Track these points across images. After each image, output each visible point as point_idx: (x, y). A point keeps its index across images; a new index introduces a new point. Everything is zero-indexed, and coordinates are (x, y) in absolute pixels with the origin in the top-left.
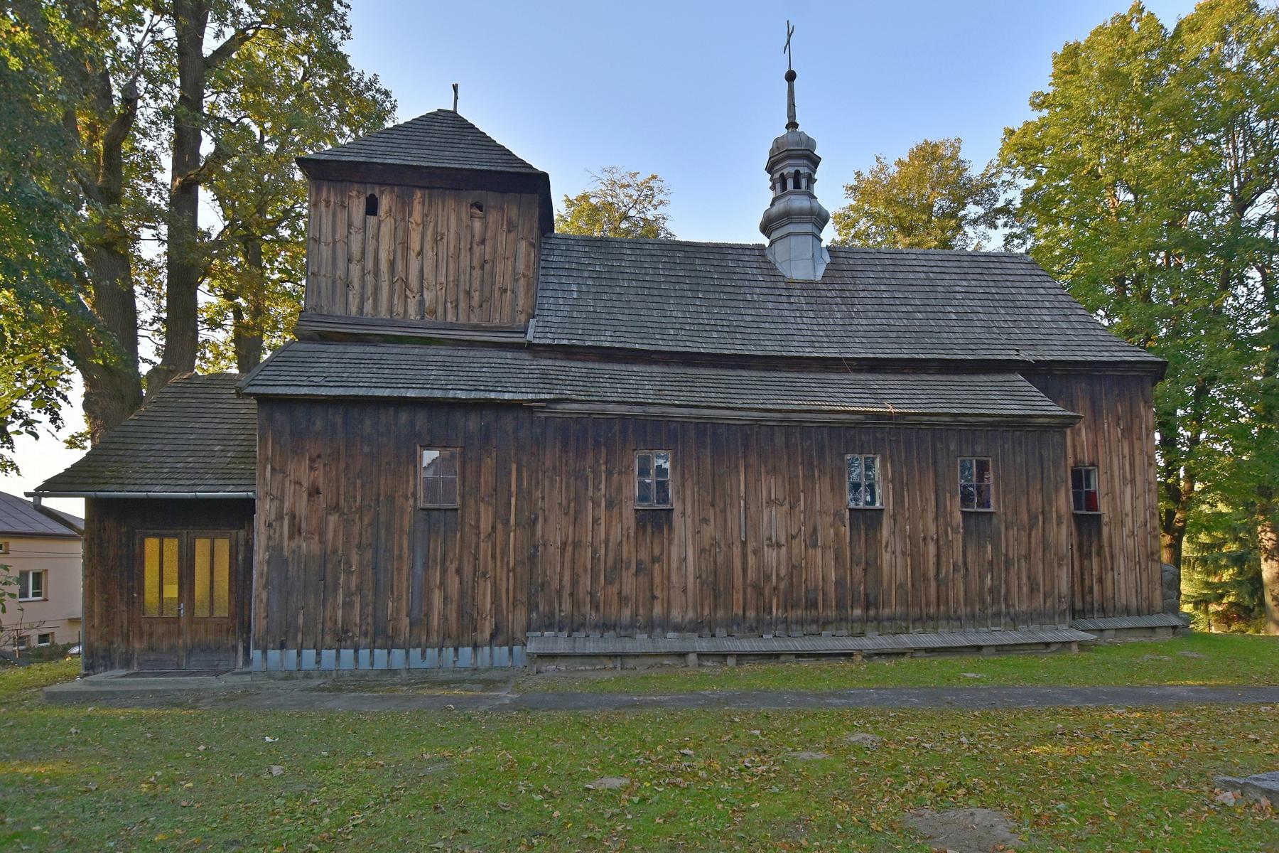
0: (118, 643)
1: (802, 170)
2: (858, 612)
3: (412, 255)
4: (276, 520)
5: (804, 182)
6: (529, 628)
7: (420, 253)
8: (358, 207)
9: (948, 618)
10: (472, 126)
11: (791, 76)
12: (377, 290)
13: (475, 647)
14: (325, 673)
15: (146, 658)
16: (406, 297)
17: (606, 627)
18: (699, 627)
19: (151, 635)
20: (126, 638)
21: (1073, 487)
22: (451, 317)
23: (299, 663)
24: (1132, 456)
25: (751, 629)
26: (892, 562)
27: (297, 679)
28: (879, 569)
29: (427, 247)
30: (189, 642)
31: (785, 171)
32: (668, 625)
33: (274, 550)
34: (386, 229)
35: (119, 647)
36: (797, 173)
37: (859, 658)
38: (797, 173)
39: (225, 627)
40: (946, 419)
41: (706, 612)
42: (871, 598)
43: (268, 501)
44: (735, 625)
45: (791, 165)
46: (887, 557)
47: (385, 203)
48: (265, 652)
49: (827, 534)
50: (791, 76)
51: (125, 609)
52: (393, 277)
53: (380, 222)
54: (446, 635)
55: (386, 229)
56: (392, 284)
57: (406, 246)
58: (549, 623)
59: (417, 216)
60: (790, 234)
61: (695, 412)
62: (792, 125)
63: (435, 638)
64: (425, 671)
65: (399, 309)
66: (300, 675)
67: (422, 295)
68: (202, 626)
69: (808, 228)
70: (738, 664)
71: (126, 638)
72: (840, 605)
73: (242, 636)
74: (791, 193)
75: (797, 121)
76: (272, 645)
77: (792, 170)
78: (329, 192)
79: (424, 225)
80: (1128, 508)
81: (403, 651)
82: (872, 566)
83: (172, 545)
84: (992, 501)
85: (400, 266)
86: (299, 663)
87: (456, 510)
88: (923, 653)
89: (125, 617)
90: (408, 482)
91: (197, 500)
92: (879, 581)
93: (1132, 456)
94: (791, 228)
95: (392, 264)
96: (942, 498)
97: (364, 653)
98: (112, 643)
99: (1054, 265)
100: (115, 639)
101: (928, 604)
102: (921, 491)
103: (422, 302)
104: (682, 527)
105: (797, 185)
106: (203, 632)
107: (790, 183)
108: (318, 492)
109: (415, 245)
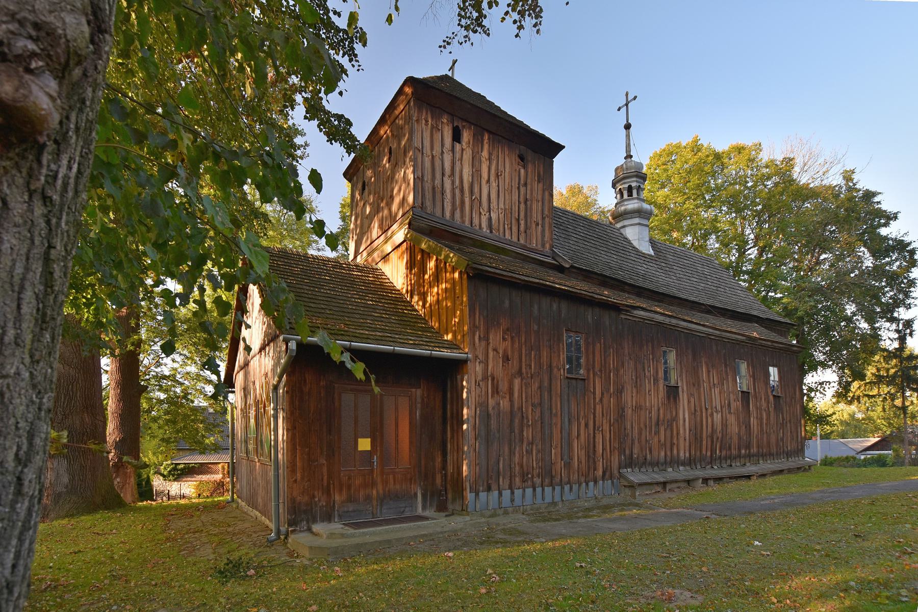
0: (321, 500)
1: (634, 185)
3: (484, 182)
4: (483, 380)
7: (488, 181)
10: (479, 94)
11: (628, 127)
12: (463, 203)
13: (596, 482)
15: (346, 509)
16: (480, 213)
18: (690, 462)
19: (349, 487)
20: (328, 492)
23: (500, 503)
27: (499, 515)
29: (492, 178)
30: (381, 492)
32: (674, 462)
33: (482, 406)
35: (319, 500)
37: (755, 478)
39: (409, 476)
43: (477, 363)
47: (466, 136)
48: (477, 495)
49: (734, 405)
50: (628, 127)
51: (325, 462)
52: (472, 196)
53: (463, 150)
59: (485, 154)
62: (629, 156)
65: (476, 221)
66: (501, 512)
67: (490, 214)
68: (391, 476)
71: (328, 492)
73: (420, 484)
74: (627, 200)
76: (481, 488)
77: (626, 186)
78: (427, 114)
79: (490, 159)
81: (551, 488)
85: (476, 189)
86: (500, 503)
87: (584, 380)
89: (325, 470)
90: (559, 356)
91: (430, 359)
94: (637, 220)
98: (314, 497)
99: (760, 267)
100: (316, 493)
104: (683, 397)
105: (630, 194)
106: (392, 481)
108: (508, 359)
109: (485, 175)
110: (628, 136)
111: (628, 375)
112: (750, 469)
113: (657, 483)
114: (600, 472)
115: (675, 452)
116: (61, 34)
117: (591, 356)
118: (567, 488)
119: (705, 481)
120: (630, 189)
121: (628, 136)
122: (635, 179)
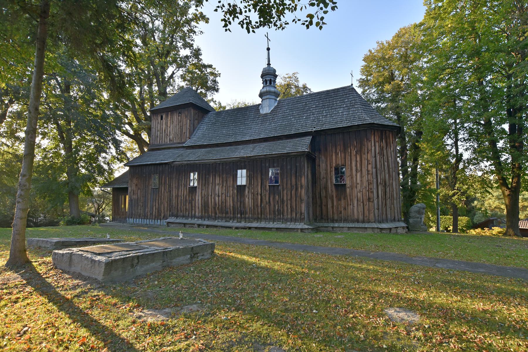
2: (239, 215)
5: (272, 83)
6: (170, 216)
8: (159, 118)
9: (264, 219)
11: (268, 49)
13: (161, 220)
14: (137, 224)
17: (183, 216)
18: (201, 218)
21: (335, 174)
22: (175, 142)
24: (361, 161)
25: (213, 219)
26: (248, 201)
28: (244, 204)
31: (267, 79)
32: (195, 217)
34: (164, 123)
36: (271, 80)
38: (271, 80)
40: (295, 154)
41: (203, 214)
42: (242, 211)
44: (209, 218)
45: (269, 77)
46: (247, 199)
47: (164, 117)
50: (268, 49)
54: (155, 217)
55: (164, 123)
56: (165, 135)
57: (167, 126)
58: (172, 215)
60: (267, 99)
61: (200, 161)
62: (269, 64)
63: (154, 217)
64: (152, 225)
65: (166, 141)
69: (274, 97)
70: (206, 228)
72: (234, 214)
74: (268, 86)
75: (270, 63)
77: (269, 79)
80: (359, 181)
82: (243, 202)
83: (123, 197)
84: (279, 181)
88: (254, 229)
92: (244, 207)
93: (361, 161)
94: (268, 97)
95: (165, 131)
96: (263, 182)
97: (138, 220)
101: (258, 214)
102: (257, 179)
103: (170, 139)
105: (270, 83)
107: (268, 82)
109: (169, 125)
110: (269, 61)
111: (174, 185)
112: (291, 225)
113: (183, 223)
114: (162, 218)
115: (193, 213)
116: (62, 154)
117: (160, 181)
118: (151, 220)
119: (199, 225)
120: (270, 81)
121: (269, 61)
122: (273, 77)
